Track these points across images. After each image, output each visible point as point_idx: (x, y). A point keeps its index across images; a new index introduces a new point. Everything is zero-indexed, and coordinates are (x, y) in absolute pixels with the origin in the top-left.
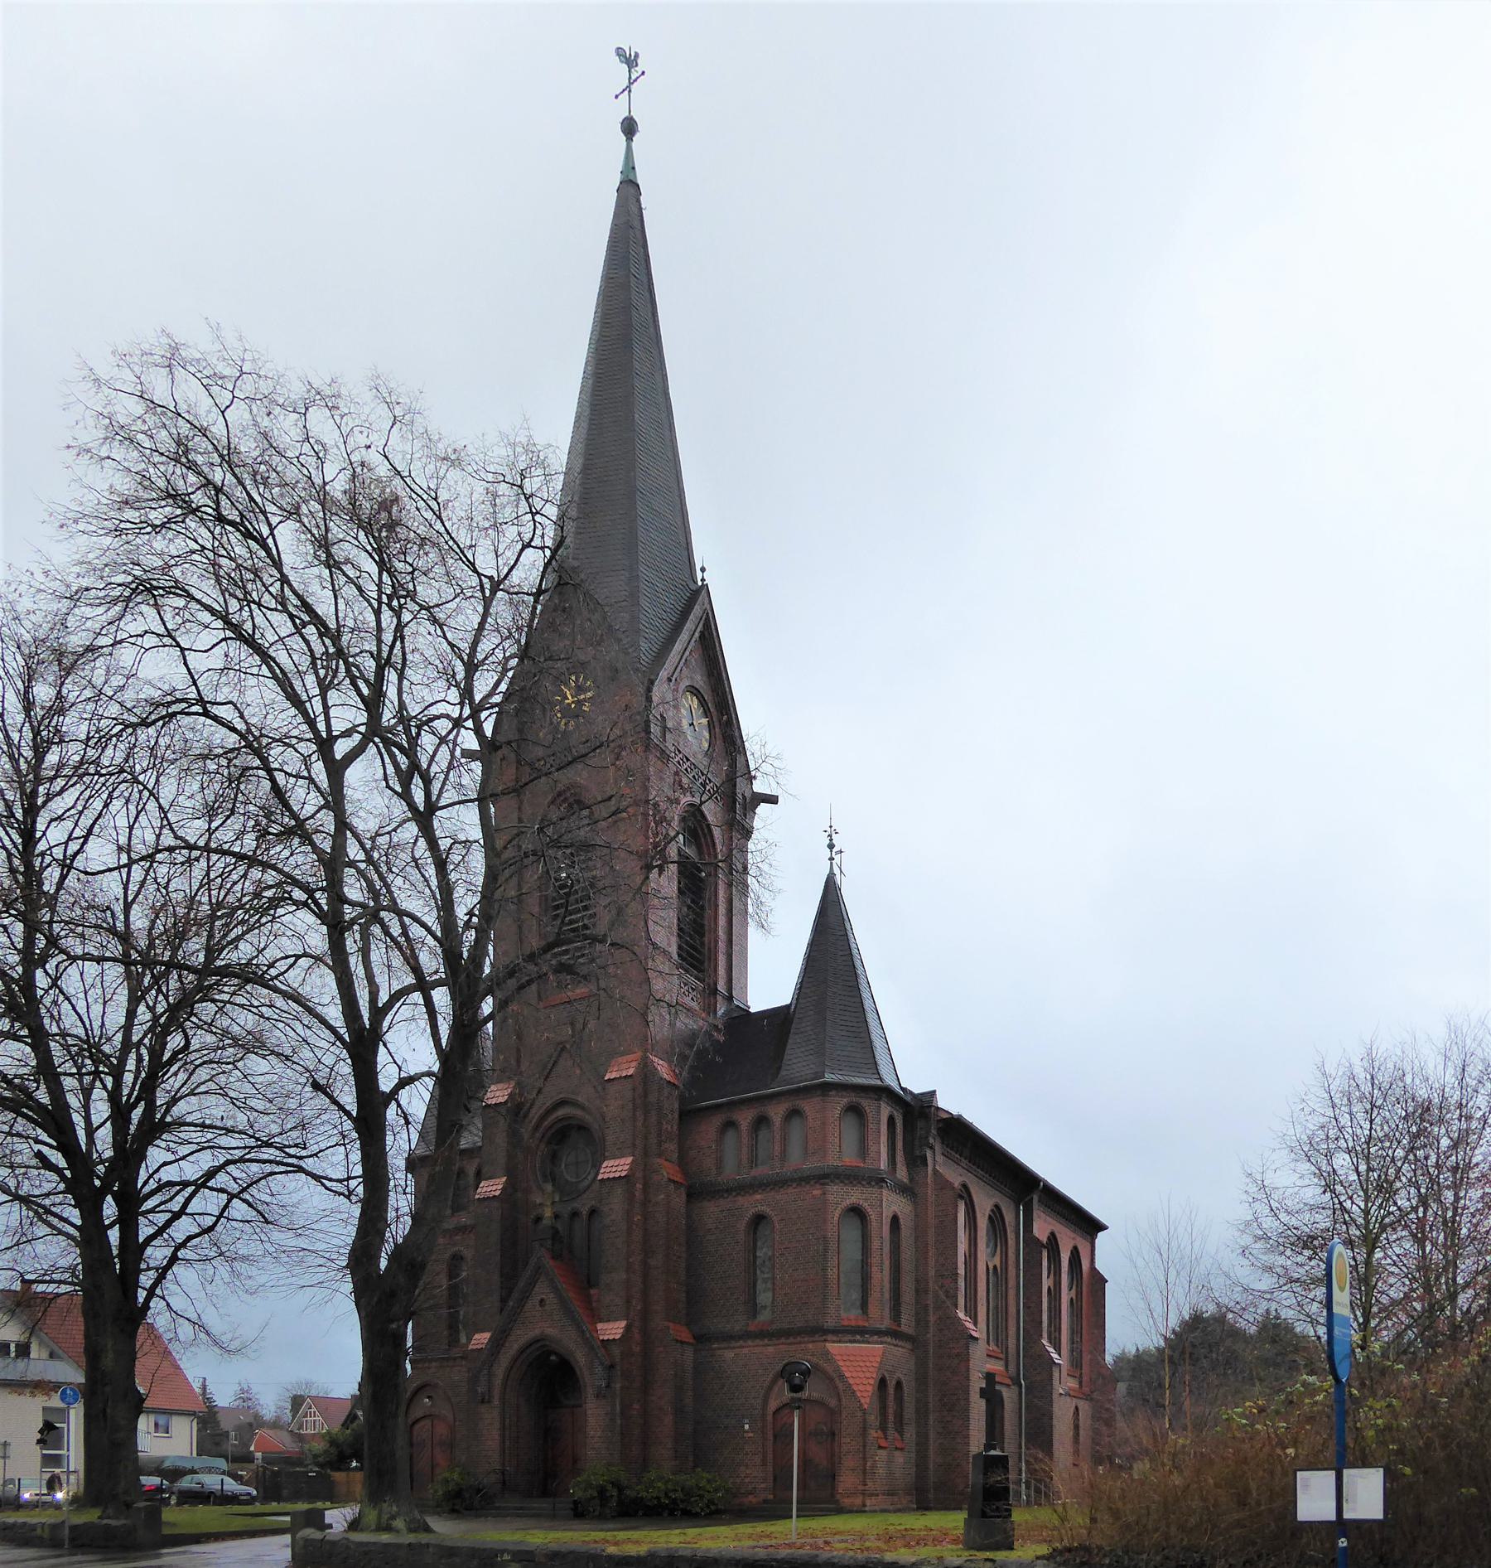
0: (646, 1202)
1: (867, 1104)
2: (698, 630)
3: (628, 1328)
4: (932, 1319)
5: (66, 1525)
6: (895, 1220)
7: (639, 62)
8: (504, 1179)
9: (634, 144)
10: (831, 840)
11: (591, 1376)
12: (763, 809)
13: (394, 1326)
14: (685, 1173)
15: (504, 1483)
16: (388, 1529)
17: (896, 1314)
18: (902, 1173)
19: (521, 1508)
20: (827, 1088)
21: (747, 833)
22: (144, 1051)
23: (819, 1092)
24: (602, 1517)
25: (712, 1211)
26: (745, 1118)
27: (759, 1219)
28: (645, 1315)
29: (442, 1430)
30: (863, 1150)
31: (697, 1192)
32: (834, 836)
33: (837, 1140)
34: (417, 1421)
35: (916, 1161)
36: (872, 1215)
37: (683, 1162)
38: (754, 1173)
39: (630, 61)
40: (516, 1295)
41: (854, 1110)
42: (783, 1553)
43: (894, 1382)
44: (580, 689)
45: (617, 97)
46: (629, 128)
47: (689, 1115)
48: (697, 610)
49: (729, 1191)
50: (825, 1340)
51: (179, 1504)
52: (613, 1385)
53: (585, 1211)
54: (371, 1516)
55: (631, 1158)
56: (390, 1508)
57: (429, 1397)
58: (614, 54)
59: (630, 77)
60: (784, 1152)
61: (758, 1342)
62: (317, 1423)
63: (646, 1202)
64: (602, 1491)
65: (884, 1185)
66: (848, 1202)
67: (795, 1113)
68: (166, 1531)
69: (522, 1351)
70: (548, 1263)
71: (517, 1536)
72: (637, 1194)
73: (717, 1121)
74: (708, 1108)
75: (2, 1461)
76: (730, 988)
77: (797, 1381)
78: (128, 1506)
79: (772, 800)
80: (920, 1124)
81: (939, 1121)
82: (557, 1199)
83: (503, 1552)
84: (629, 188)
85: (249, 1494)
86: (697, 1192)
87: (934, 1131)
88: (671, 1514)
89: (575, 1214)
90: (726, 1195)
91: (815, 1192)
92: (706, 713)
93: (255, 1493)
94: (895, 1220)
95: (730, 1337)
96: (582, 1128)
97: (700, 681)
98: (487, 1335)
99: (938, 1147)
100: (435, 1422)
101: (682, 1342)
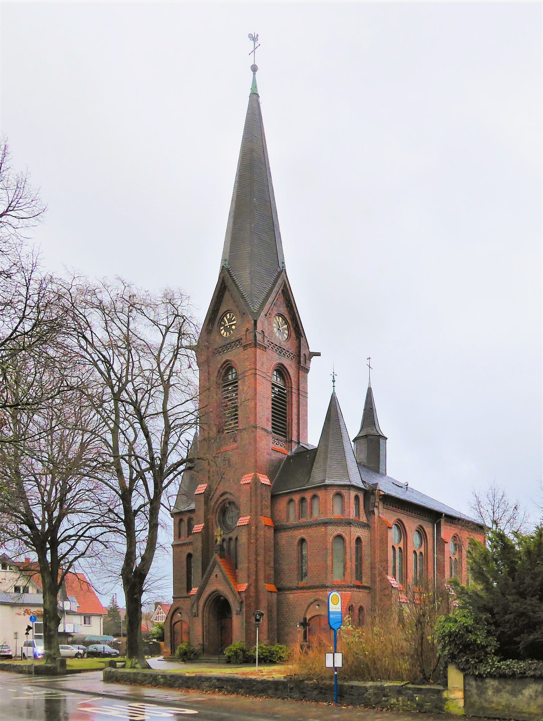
0: (256, 534)
1: (344, 492)
2: (281, 289)
3: (249, 587)
4: (378, 579)
5: (33, 666)
6: (358, 540)
7: (258, 38)
8: (203, 524)
9: (256, 76)
10: (334, 378)
11: (235, 607)
12: (314, 359)
13: (135, 596)
14: (274, 521)
15: (203, 649)
16: (134, 667)
17: (359, 577)
18: (363, 519)
19: (208, 660)
20: (326, 486)
21: (307, 371)
22: (58, 486)
23: (324, 488)
24: (236, 663)
25: (284, 537)
26: (296, 498)
27: (302, 541)
28: (257, 580)
29: (185, 627)
30: (343, 511)
31: (277, 529)
32: (335, 376)
33: (331, 508)
34: (176, 622)
35: (370, 513)
36: (347, 538)
37: (272, 517)
38: (300, 521)
39: (254, 39)
40: (206, 574)
41: (339, 494)
42: (227, 675)
43: (358, 607)
44: (230, 320)
45: (249, 54)
46: (254, 69)
47: (274, 497)
48: (280, 281)
49: (291, 528)
50: (327, 591)
51: (88, 657)
52: (242, 610)
53: (227, 539)
54: (129, 663)
55: (250, 517)
56: (135, 660)
57: (180, 613)
58: (247, 37)
59: (254, 47)
60: (312, 513)
61: (302, 591)
62: (163, 617)
63: (256, 534)
64: (236, 653)
65: (352, 525)
66: (336, 533)
67: (315, 496)
68: (68, 668)
69: (210, 595)
70: (219, 560)
71: (196, 670)
72: (252, 531)
73: (286, 499)
74: (282, 494)
75: (15, 640)
76: (299, 438)
77: (258, 618)
78: (55, 659)
79: (318, 354)
80: (372, 497)
81: (380, 495)
82: (222, 533)
83: (159, 675)
84: (254, 96)
85: (116, 653)
86: (277, 529)
87: (378, 500)
88: (265, 662)
89: (230, 539)
90: (290, 530)
91: (322, 530)
92: (286, 323)
93: (118, 652)
94: (358, 540)
95: (290, 589)
96: (231, 503)
97: (283, 310)
98: (197, 588)
99: (381, 506)
100: (183, 623)
101: (271, 592)
